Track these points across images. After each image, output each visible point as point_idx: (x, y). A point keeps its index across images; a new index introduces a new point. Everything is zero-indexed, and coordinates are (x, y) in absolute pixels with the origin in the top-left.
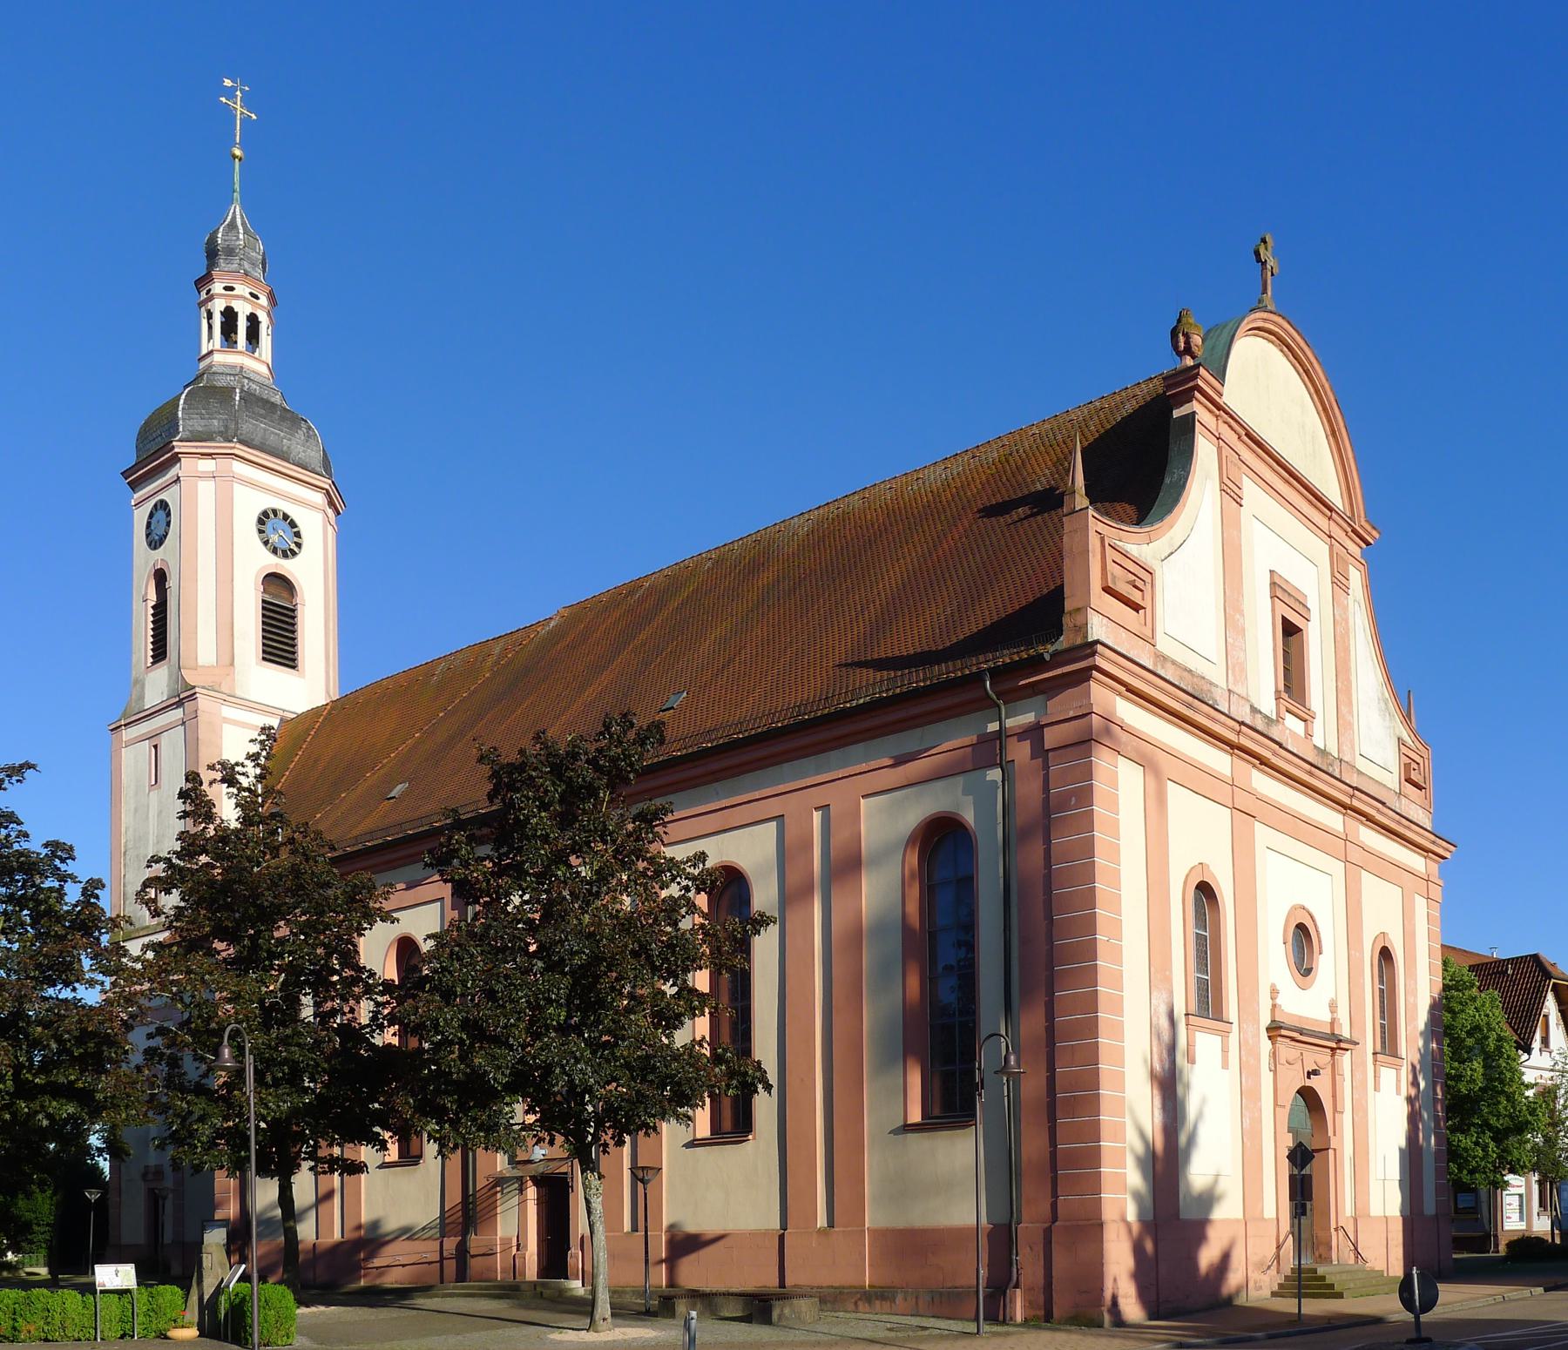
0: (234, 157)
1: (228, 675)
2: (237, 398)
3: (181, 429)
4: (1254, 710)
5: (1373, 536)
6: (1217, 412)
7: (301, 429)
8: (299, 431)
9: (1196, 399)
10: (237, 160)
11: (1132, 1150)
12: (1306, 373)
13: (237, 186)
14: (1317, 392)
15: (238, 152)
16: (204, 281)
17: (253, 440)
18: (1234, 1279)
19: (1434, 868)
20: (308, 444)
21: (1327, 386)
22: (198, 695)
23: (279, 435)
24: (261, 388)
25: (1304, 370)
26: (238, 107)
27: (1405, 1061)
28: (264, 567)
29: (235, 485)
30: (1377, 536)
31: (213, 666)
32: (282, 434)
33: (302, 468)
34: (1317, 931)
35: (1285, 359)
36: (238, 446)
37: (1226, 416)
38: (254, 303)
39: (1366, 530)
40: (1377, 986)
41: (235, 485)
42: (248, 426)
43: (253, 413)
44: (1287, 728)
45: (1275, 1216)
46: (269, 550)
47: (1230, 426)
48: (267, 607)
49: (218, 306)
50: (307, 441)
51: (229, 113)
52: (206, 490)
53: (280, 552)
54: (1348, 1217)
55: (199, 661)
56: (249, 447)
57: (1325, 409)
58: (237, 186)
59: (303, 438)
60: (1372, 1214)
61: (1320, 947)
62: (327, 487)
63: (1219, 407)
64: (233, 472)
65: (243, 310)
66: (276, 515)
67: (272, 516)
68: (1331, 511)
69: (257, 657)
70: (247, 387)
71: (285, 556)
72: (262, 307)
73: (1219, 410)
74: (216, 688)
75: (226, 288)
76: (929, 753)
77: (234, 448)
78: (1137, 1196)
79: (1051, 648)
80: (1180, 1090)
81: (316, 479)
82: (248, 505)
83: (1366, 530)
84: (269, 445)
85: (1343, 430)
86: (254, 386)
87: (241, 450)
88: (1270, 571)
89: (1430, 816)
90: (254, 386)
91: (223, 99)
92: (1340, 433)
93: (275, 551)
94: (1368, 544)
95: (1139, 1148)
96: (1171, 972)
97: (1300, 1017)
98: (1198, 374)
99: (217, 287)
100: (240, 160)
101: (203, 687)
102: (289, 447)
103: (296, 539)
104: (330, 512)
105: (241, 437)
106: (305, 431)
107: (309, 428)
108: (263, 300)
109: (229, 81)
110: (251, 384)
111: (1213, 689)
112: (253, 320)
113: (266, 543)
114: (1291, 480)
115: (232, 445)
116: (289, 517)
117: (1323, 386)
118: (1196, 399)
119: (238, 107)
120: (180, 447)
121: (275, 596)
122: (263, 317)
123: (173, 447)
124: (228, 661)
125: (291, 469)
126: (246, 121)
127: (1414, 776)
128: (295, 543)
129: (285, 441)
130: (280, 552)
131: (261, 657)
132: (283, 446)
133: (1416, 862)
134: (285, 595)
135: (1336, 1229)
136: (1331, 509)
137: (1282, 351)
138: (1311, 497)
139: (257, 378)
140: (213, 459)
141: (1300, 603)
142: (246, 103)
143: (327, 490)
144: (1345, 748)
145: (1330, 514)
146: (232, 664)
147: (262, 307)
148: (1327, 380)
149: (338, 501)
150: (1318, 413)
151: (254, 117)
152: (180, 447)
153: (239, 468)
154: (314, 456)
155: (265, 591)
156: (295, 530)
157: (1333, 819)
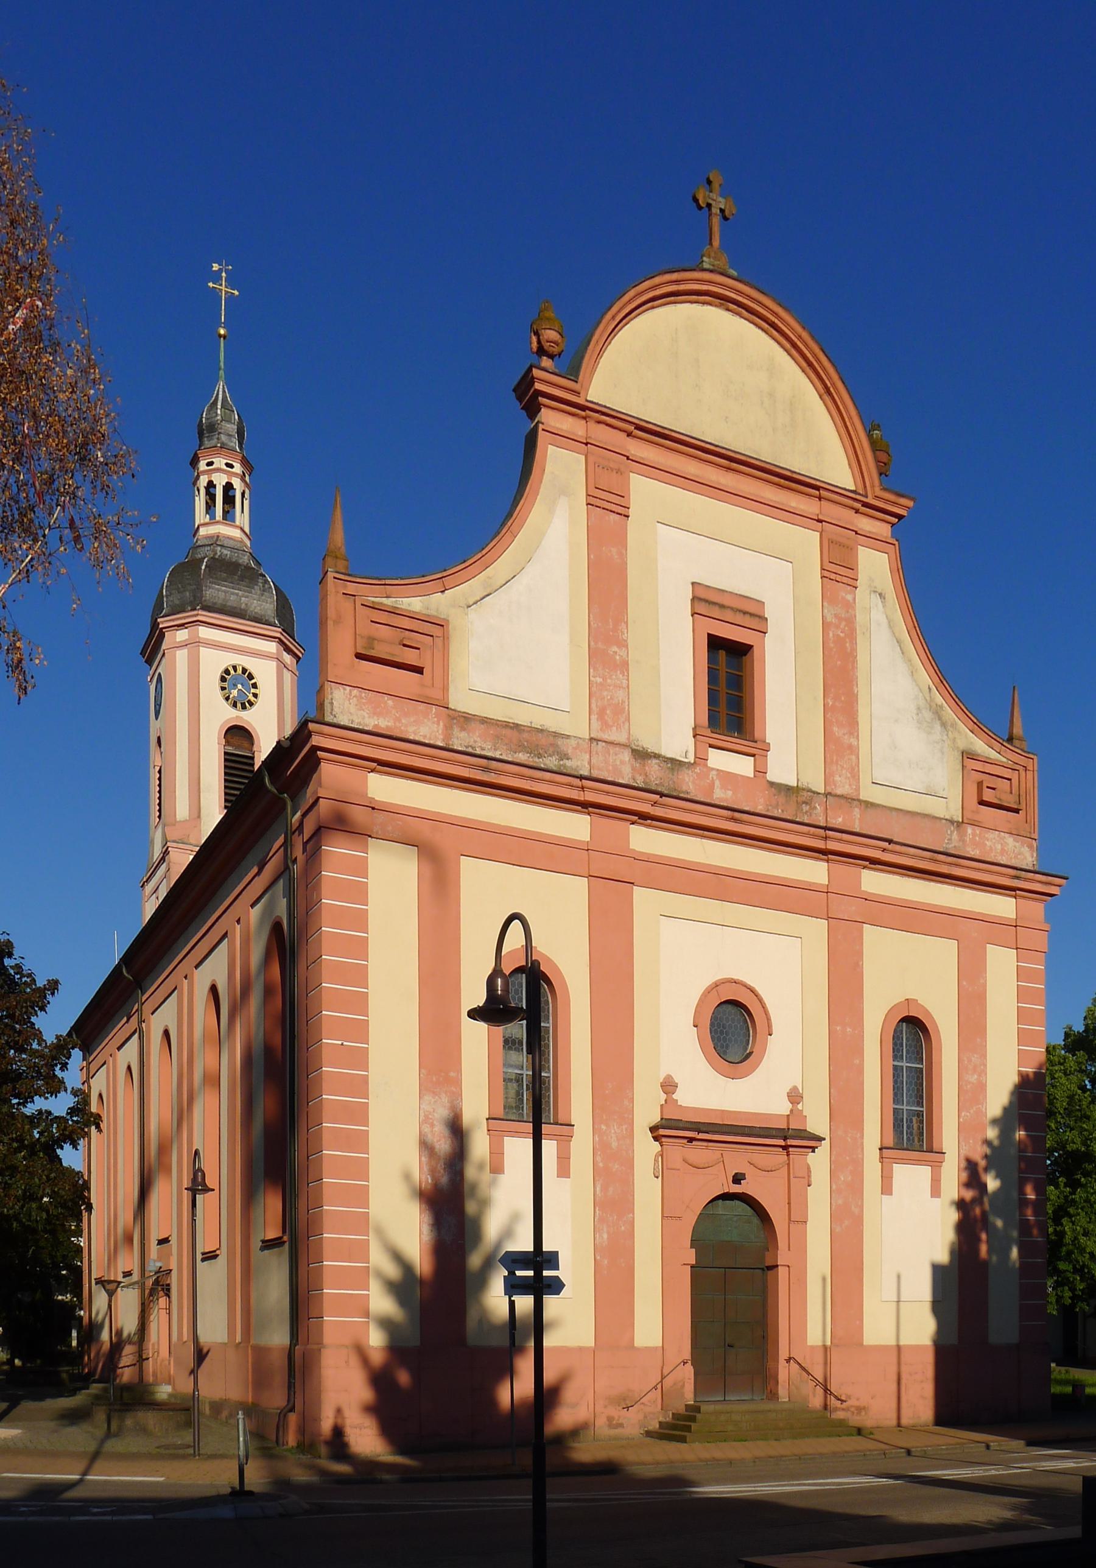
0: (220, 336)
1: (195, 827)
2: (203, 567)
3: (165, 606)
4: (641, 755)
5: (903, 506)
6: (583, 413)
7: (257, 585)
8: (256, 587)
9: (545, 406)
10: (222, 339)
11: (379, 1275)
12: (772, 327)
13: (222, 364)
14: (793, 347)
15: (222, 332)
16: (194, 462)
17: (215, 604)
18: (564, 1418)
19: (1036, 909)
20: (263, 598)
21: (805, 335)
22: (170, 849)
23: (237, 595)
24: (231, 551)
25: (769, 324)
26: (223, 288)
27: (819, 1161)
28: (226, 722)
29: (201, 648)
30: (911, 504)
31: (186, 820)
32: (240, 593)
33: (256, 622)
34: (763, 1007)
35: (737, 319)
36: (200, 612)
37: (597, 415)
38: (229, 472)
39: (887, 501)
40: (890, 1062)
41: (201, 648)
42: (216, 592)
43: (216, 578)
44: (713, 769)
45: (661, 1345)
46: (230, 705)
47: (608, 425)
48: (229, 758)
49: (203, 481)
50: (262, 595)
51: (215, 293)
52: (182, 656)
53: (239, 705)
54: (812, 1347)
55: (177, 817)
56: (209, 611)
57: (810, 364)
58: (222, 364)
59: (259, 592)
60: (865, 1343)
61: (769, 1026)
62: (278, 635)
63: (583, 408)
64: (199, 637)
65: (220, 480)
66: (235, 671)
67: (232, 672)
68: (819, 490)
69: (220, 806)
70: (219, 554)
71: (244, 707)
72: (236, 475)
73: (584, 411)
74: (185, 841)
75: (228, 465)
76: (270, 855)
77: (198, 615)
78: (386, 1324)
79: (390, 724)
80: (471, 1207)
81: (254, 627)
82: (213, 663)
83: (887, 501)
84: (229, 606)
85: (839, 384)
86: (225, 552)
87: (203, 616)
88: (693, 584)
89: (1034, 843)
90: (225, 552)
91: (211, 285)
92: (836, 388)
93: (235, 705)
94: (900, 517)
95: (392, 1271)
96: (459, 1071)
97: (723, 1111)
98: (533, 378)
99: (202, 465)
100: (225, 337)
101: (174, 841)
102: (246, 604)
103: (253, 690)
104: (287, 658)
105: (205, 603)
106: (261, 585)
107: (266, 581)
108: (238, 468)
109: (217, 265)
110: (223, 550)
111: (560, 742)
112: (229, 487)
113: (227, 699)
114: (734, 465)
115: (195, 612)
116: (247, 670)
117: (800, 337)
118: (545, 406)
119: (223, 288)
120: (162, 622)
121: (238, 747)
122: (237, 483)
123: (159, 624)
124: (196, 815)
125: (254, 627)
126: (230, 298)
127: (988, 796)
128: (253, 694)
129: (243, 599)
130: (239, 705)
131: (223, 806)
132: (241, 604)
133: (1003, 906)
134: (246, 744)
135: (788, 1361)
136: (817, 488)
137: (728, 310)
138: (776, 479)
139: (231, 543)
140: (186, 628)
141: (751, 615)
142: (231, 283)
143: (279, 639)
144: (837, 778)
145: (817, 492)
146: (199, 817)
147: (236, 475)
148: (804, 328)
149: (295, 646)
150: (803, 371)
151: (236, 293)
152: (162, 622)
153: (204, 632)
154: (267, 606)
155: (228, 743)
156: (253, 681)
157: (815, 871)
